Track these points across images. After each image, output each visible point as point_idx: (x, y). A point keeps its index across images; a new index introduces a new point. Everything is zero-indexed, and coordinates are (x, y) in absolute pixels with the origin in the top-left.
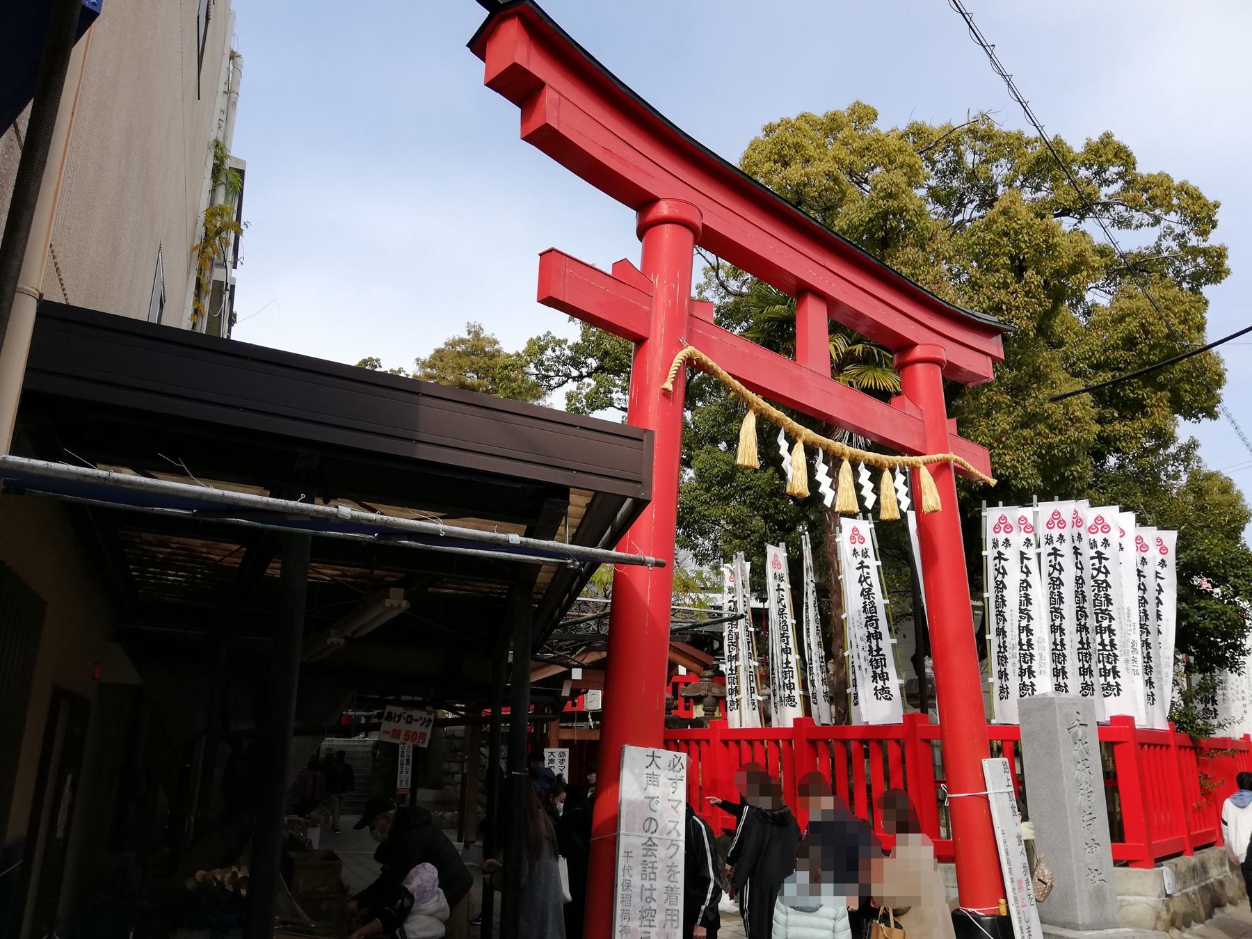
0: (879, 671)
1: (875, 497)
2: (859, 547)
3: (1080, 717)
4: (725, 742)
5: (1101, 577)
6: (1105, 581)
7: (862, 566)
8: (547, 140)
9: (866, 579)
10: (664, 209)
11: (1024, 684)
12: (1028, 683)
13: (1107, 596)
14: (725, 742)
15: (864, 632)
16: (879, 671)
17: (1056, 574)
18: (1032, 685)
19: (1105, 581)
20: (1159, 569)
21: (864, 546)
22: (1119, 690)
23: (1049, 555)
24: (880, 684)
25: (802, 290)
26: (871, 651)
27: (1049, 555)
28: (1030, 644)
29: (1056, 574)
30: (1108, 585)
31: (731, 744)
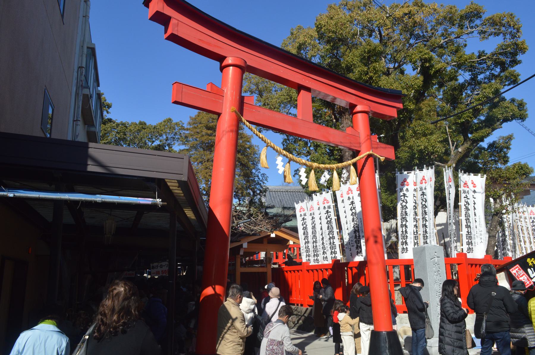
0: (333, 251)
1: (307, 180)
2: (326, 205)
3: (436, 254)
4: (308, 271)
5: (404, 204)
6: (405, 206)
7: (327, 212)
8: (174, 38)
9: (329, 217)
10: (229, 60)
11: (403, 248)
12: (405, 247)
13: (406, 212)
14: (308, 271)
15: (304, 241)
16: (333, 251)
17: (424, 203)
18: (407, 248)
19: (405, 206)
20: (414, 193)
21: (329, 204)
22: (407, 250)
23: (465, 197)
24: (316, 258)
25: (300, 88)
26: (330, 243)
27: (465, 197)
28: (406, 232)
29: (424, 203)
30: (407, 207)
31: (310, 271)
